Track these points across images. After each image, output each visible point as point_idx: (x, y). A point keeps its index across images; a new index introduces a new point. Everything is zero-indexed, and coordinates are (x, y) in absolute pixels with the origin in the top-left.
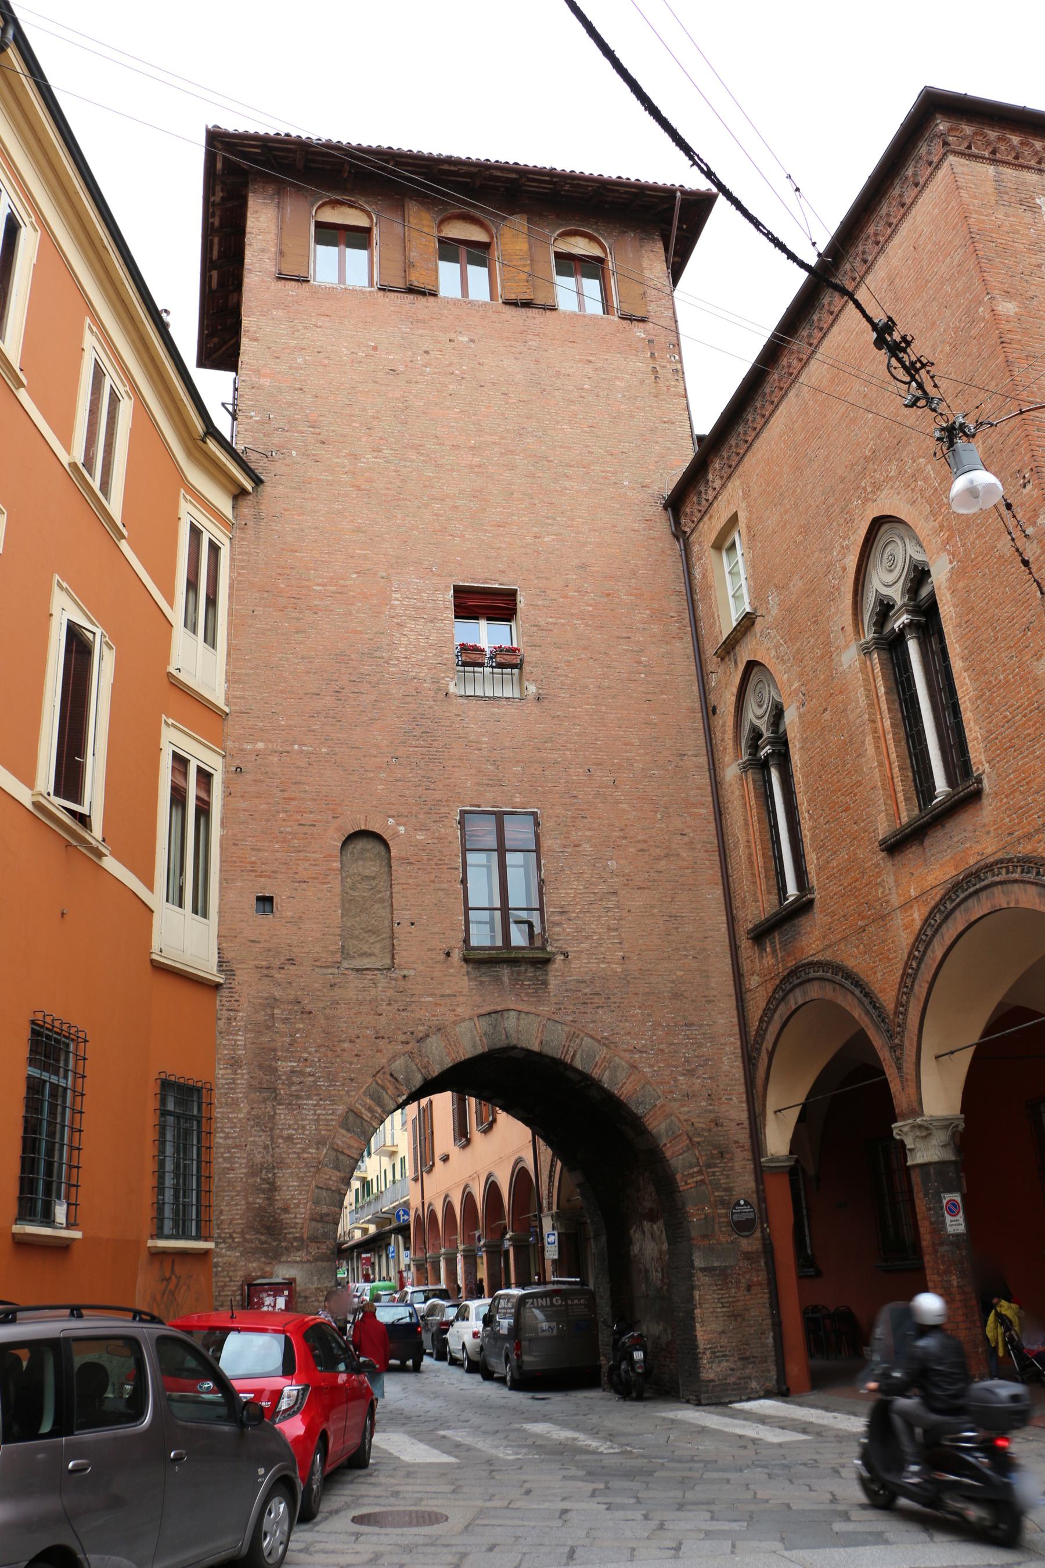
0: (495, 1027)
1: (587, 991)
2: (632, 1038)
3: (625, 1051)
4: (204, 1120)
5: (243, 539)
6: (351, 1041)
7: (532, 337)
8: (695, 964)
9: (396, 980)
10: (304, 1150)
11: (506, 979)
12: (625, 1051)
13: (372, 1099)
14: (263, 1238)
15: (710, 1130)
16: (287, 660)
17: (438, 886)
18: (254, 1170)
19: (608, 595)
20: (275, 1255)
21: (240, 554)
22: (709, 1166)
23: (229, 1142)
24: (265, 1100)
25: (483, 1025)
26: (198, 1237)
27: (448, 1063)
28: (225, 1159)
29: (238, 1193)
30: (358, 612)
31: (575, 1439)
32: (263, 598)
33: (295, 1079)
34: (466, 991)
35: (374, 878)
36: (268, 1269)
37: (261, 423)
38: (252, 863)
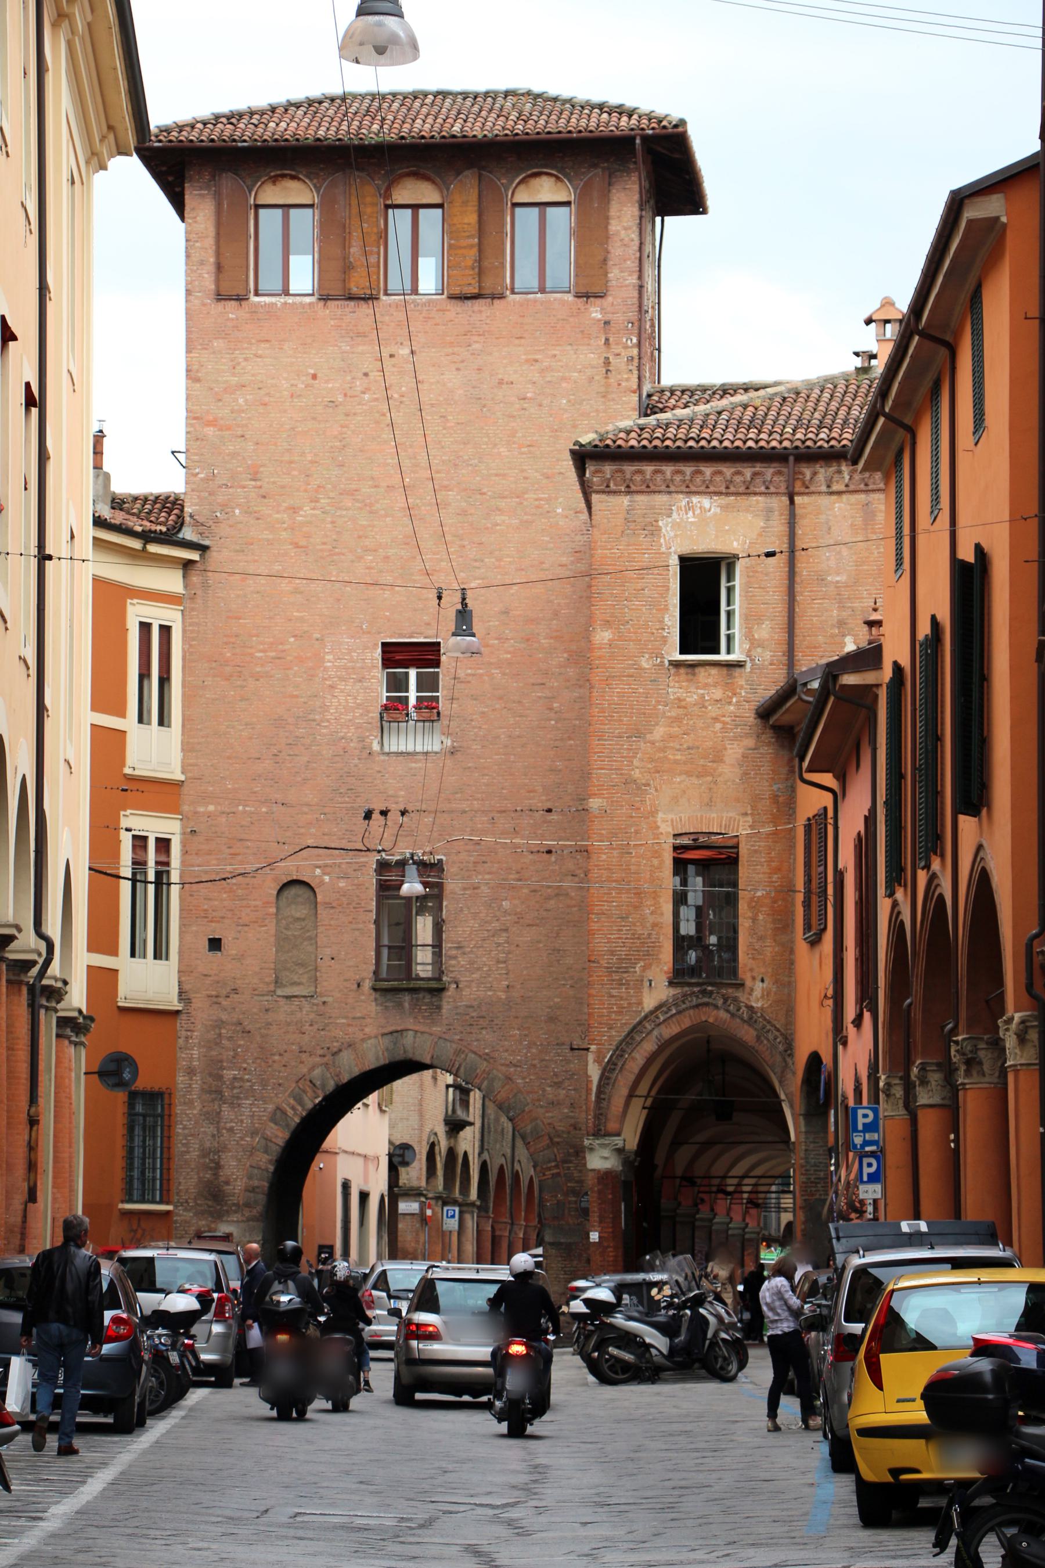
0: (395, 1044)
1: (474, 1014)
2: (510, 1055)
3: (502, 1065)
4: (166, 1117)
5: (193, 609)
6: (280, 1055)
7: (476, 338)
8: (571, 993)
9: (317, 1005)
10: (242, 1139)
11: (407, 1005)
12: (502, 1065)
13: (295, 1099)
14: (210, 1203)
15: (569, 1133)
16: (233, 727)
17: (354, 926)
18: (205, 1153)
19: (528, 640)
20: (219, 1216)
21: (190, 625)
22: (565, 1162)
23: (186, 1131)
24: (213, 1100)
25: (386, 1042)
26: (161, 1202)
27: (356, 1072)
28: (183, 1144)
29: (192, 1170)
30: (294, 677)
31: (794, 1073)
32: (211, 668)
33: (236, 1084)
34: (373, 1015)
35: (304, 919)
36: (213, 1226)
37: (206, 480)
38: (206, 910)
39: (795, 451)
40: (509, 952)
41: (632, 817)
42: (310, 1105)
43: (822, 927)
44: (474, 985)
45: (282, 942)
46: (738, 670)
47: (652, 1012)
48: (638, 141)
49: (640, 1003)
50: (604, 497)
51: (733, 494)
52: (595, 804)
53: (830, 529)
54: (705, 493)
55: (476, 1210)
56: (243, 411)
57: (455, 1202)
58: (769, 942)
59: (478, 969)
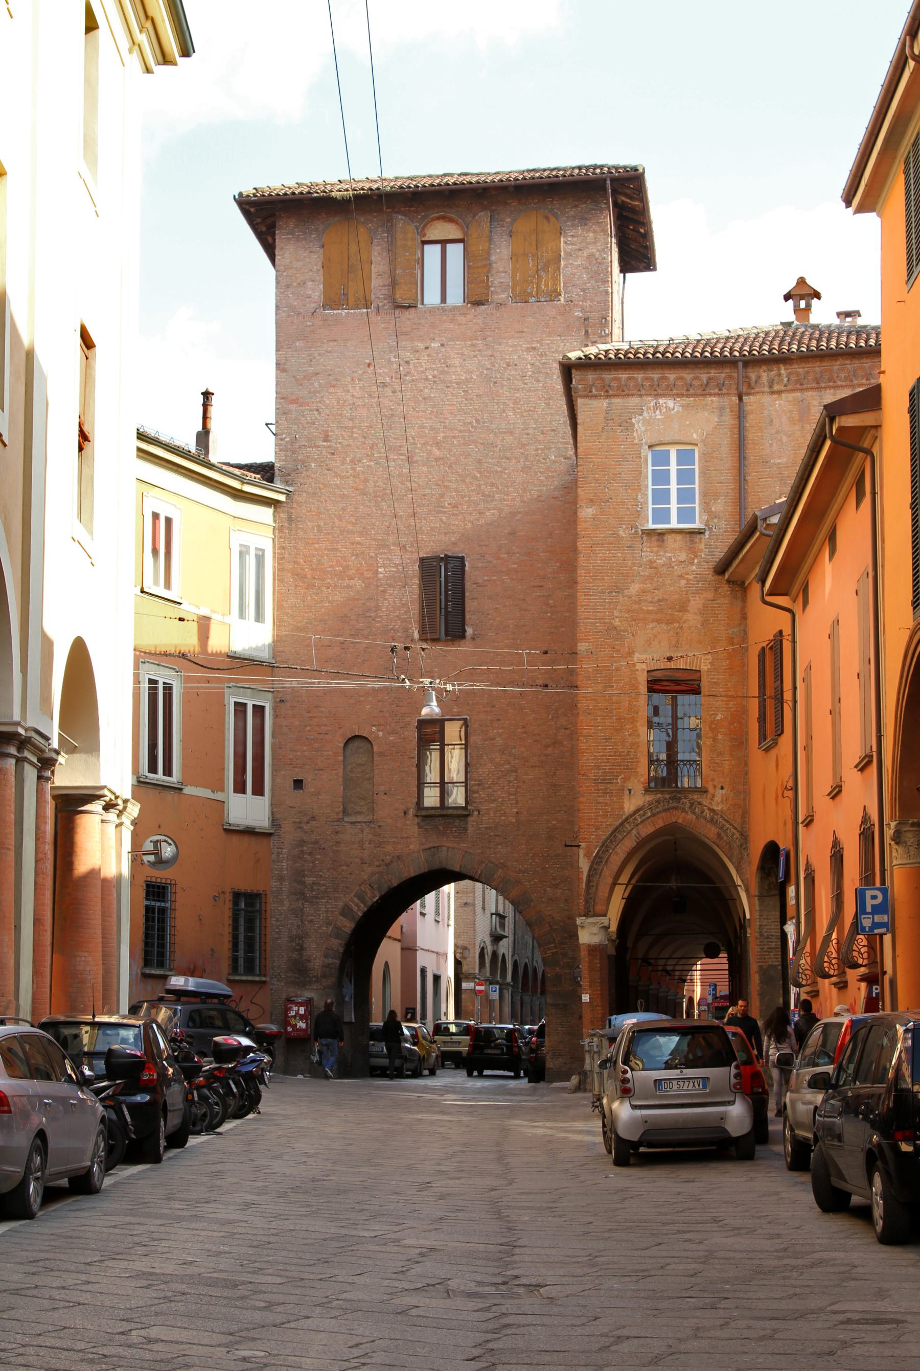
10: (319, 928)
24: (298, 900)
26: (259, 975)
34: (416, 835)
35: (364, 765)
39: (743, 358)
40: (518, 787)
41: (613, 657)
42: (370, 903)
43: (779, 732)
44: (491, 812)
45: (348, 782)
46: (698, 536)
47: (631, 816)
48: (608, 182)
49: (622, 808)
50: (587, 401)
51: (692, 396)
52: (582, 647)
53: (772, 421)
54: (670, 395)
55: (510, 988)
56: (318, 392)
57: (497, 983)
58: (727, 757)
59: (494, 800)
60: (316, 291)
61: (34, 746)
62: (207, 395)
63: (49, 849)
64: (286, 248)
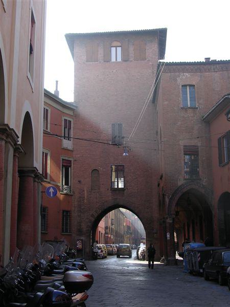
60: (84, 58)
61: (12, 136)
62: (57, 82)
63: (17, 196)
64: (76, 50)
